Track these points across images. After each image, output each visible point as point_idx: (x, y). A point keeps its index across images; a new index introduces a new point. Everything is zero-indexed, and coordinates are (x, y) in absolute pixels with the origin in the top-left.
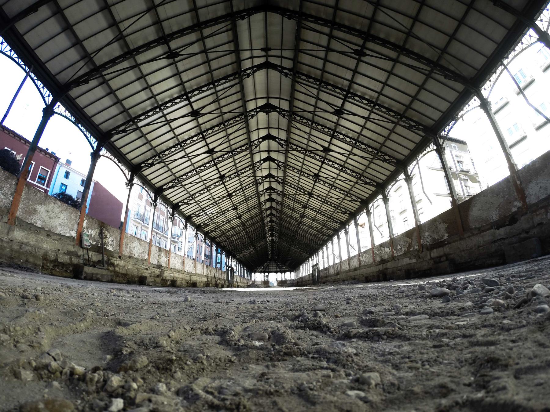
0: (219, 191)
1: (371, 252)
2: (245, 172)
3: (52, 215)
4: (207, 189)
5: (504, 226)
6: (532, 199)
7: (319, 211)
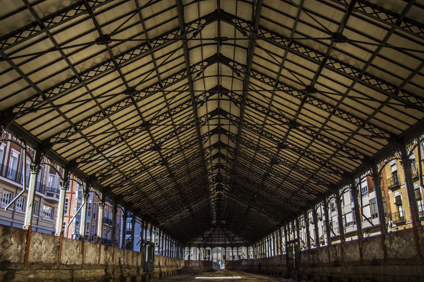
2: (174, 83)
4: (104, 113)
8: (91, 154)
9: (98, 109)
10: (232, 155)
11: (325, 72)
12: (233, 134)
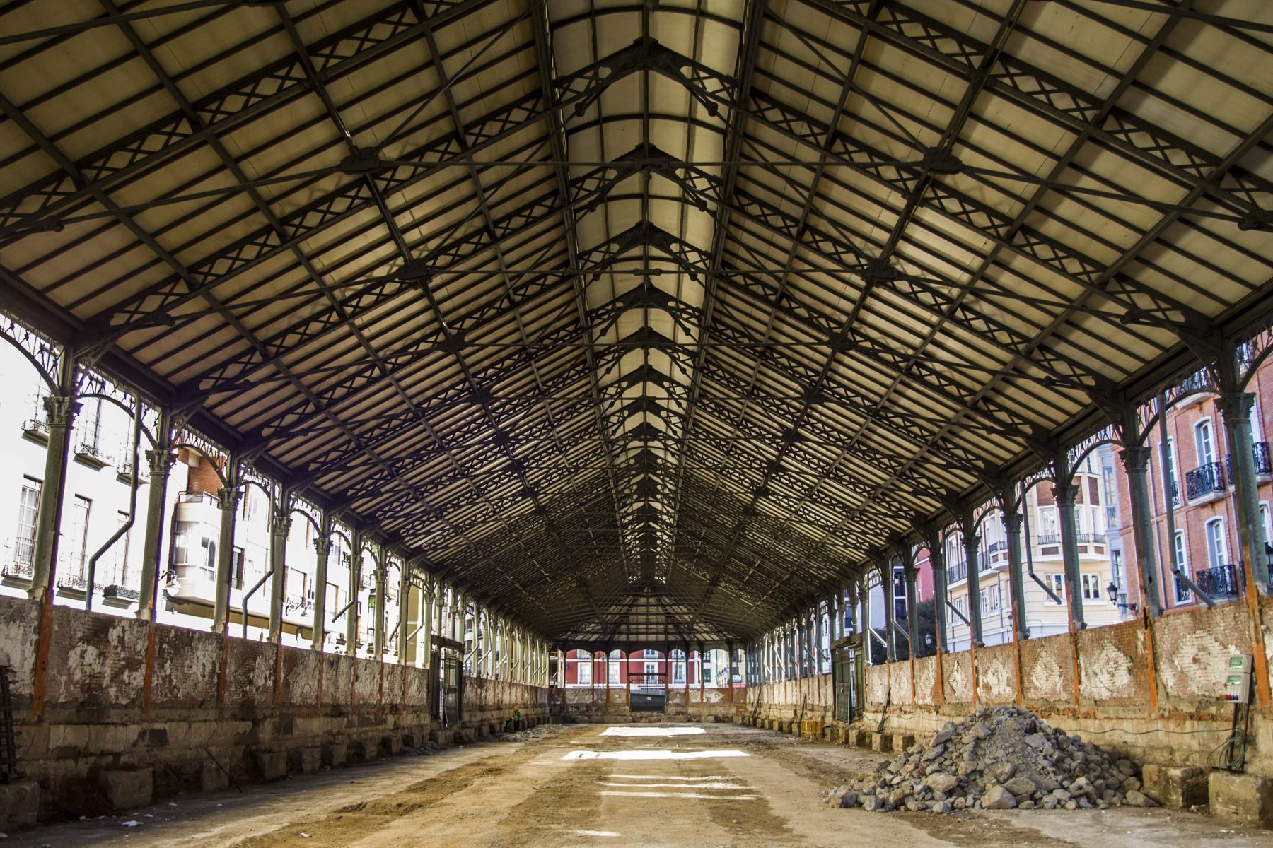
8: (246, 364)
9: (259, 220)
10: (683, 371)
12: (689, 307)
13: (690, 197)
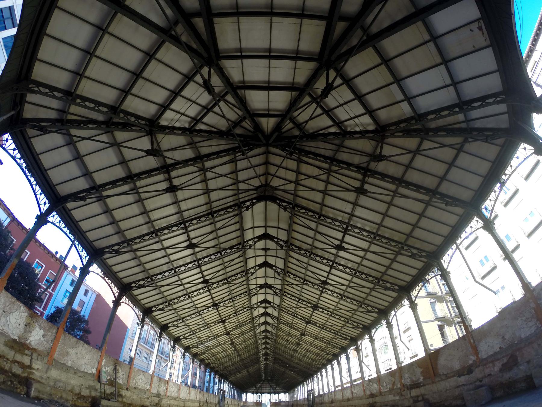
0: (211, 315)
1: (362, 385)
3: (80, 356)
5: (464, 375)
6: (483, 355)
7: (323, 327)
11: (334, 271)
13: (276, 294)
